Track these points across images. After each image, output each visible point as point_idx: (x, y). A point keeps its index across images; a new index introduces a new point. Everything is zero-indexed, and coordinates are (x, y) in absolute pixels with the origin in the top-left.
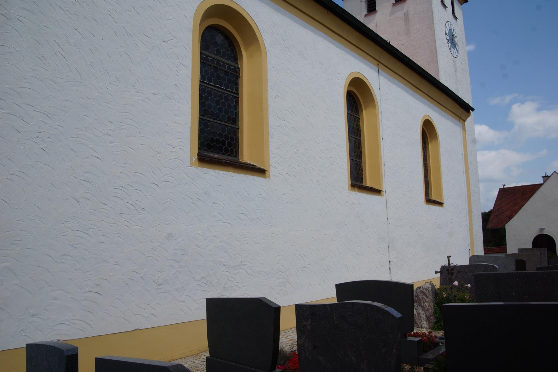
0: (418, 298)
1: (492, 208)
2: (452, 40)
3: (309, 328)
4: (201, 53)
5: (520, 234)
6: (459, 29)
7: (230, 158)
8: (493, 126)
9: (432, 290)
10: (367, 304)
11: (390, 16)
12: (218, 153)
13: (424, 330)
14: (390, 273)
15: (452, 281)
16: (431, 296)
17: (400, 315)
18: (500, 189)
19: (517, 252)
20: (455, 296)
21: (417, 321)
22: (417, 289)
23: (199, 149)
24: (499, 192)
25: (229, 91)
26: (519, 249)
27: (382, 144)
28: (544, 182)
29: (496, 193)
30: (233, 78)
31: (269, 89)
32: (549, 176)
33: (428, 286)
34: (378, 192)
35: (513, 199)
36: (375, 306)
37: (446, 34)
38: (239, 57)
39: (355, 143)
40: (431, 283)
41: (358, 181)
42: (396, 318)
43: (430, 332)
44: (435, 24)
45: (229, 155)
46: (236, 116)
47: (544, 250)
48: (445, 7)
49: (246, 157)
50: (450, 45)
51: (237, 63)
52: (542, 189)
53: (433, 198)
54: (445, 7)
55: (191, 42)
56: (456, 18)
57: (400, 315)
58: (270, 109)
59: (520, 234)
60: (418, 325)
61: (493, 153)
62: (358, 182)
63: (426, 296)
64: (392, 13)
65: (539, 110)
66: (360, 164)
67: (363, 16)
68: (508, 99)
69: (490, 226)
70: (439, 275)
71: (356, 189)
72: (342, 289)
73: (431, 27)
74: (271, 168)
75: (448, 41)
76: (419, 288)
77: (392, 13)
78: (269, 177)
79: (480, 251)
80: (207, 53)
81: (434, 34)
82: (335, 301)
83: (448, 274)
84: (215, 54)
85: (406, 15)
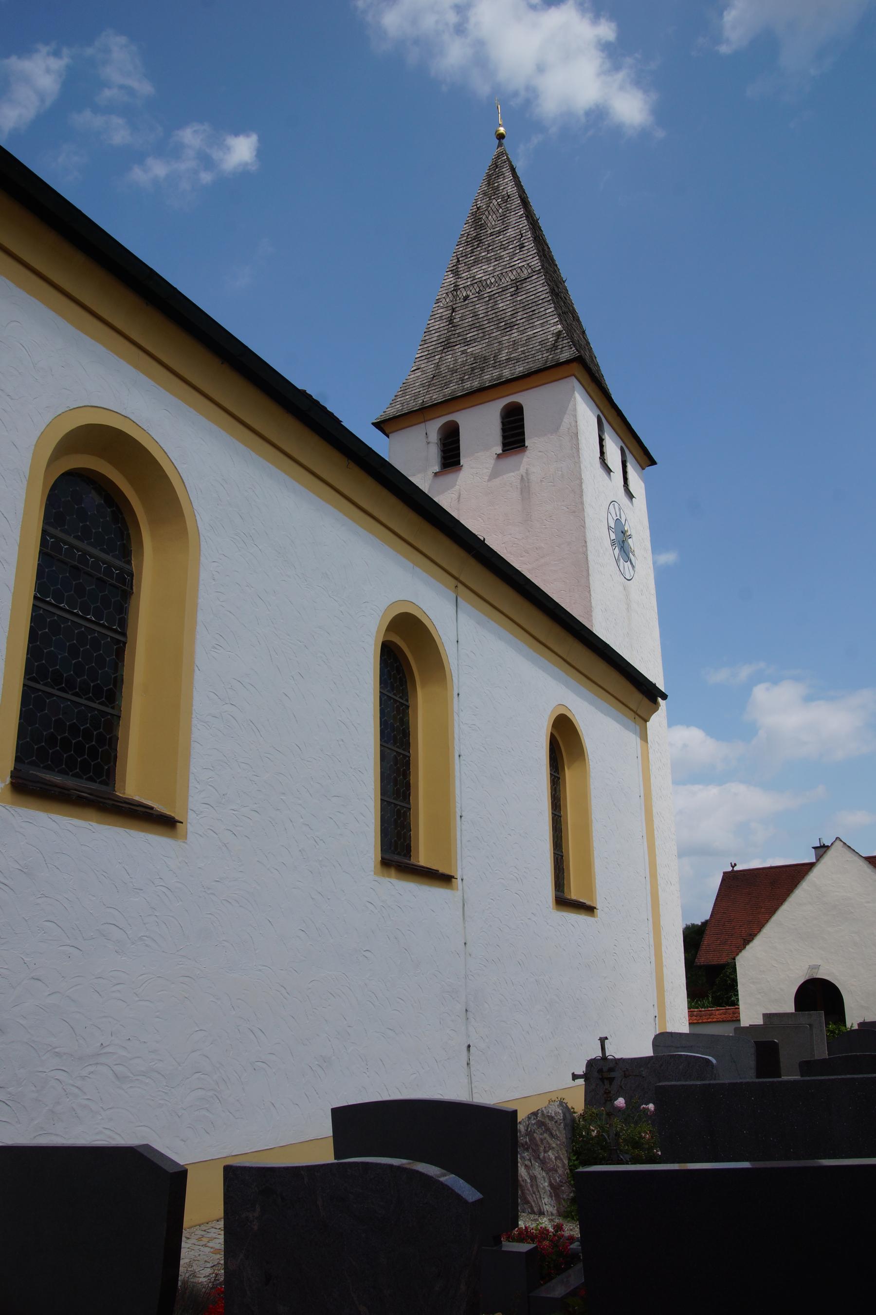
0: (532, 1139)
1: (708, 918)
2: (622, 542)
3: (256, 1228)
4: (44, 532)
5: (766, 981)
6: (637, 518)
7: (94, 786)
8: (716, 728)
9: (564, 1119)
10: (399, 1168)
11: (489, 480)
12: (62, 772)
13: (545, 1222)
14: (470, 1076)
15: (610, 1098)
16: (561, 1133)
17: (478, 1196)
18: (725, 873)
19: (761, 1022)
20: (617, 1135)
21: (529, 1198)
22: (529, 1118)
23: (18, 759)
24: (723, 880)
25: (103, 626)
26: (765, 1015)
27: (457, 767)
28: (819, 858)
29: (716, 881)
30: (115, 594)
31: (200, 628)
32: (828, 847)
33: (555, 1110)
34: (445, 879)
35: (753, 896)
36: (417, 1172)
37: (609, 528)
38: (134, 548)
39: (396, 764)
40: (562, 1103)
41: (398, 850)
42: (466, 1202)
43: (558, 1228)
44: (586, 505)
45: (91, 779)
46: (115, 685)
47: (819, 1016)
48: (608, 470)
49: (133, 786)
50: (617, 551)
51: (129, 562)
52: (813, 876)
53: (574, 894)
54: (608, 470)
55: (21, 506)
56: (630, 496)
57: (478, 1196)
58: (198, 676)
59: (766, 981)
60: (531, 1207)
61: (713, 791)
62: (399, 854)
63: (552, 1135)
64: (494, 475)
65: (808, 699)
66: (405, 813)
67: (430, 475)
68: (745, 672)
69: (702, 959)
70: (581, 1082)
71: (393, 871)
72: (350, 1122)
73: (577, 509)
74: (191, 816)
75: (613, 543)
76: (535, 1114)
77: (494, 475)
78: (185, 837)
79: (679, 1020)
80: (52, 530)
81: (584, 527)
82: (326, 1156)
83: (602, 1079)
84: (76, 537)
85: (525, 480)
